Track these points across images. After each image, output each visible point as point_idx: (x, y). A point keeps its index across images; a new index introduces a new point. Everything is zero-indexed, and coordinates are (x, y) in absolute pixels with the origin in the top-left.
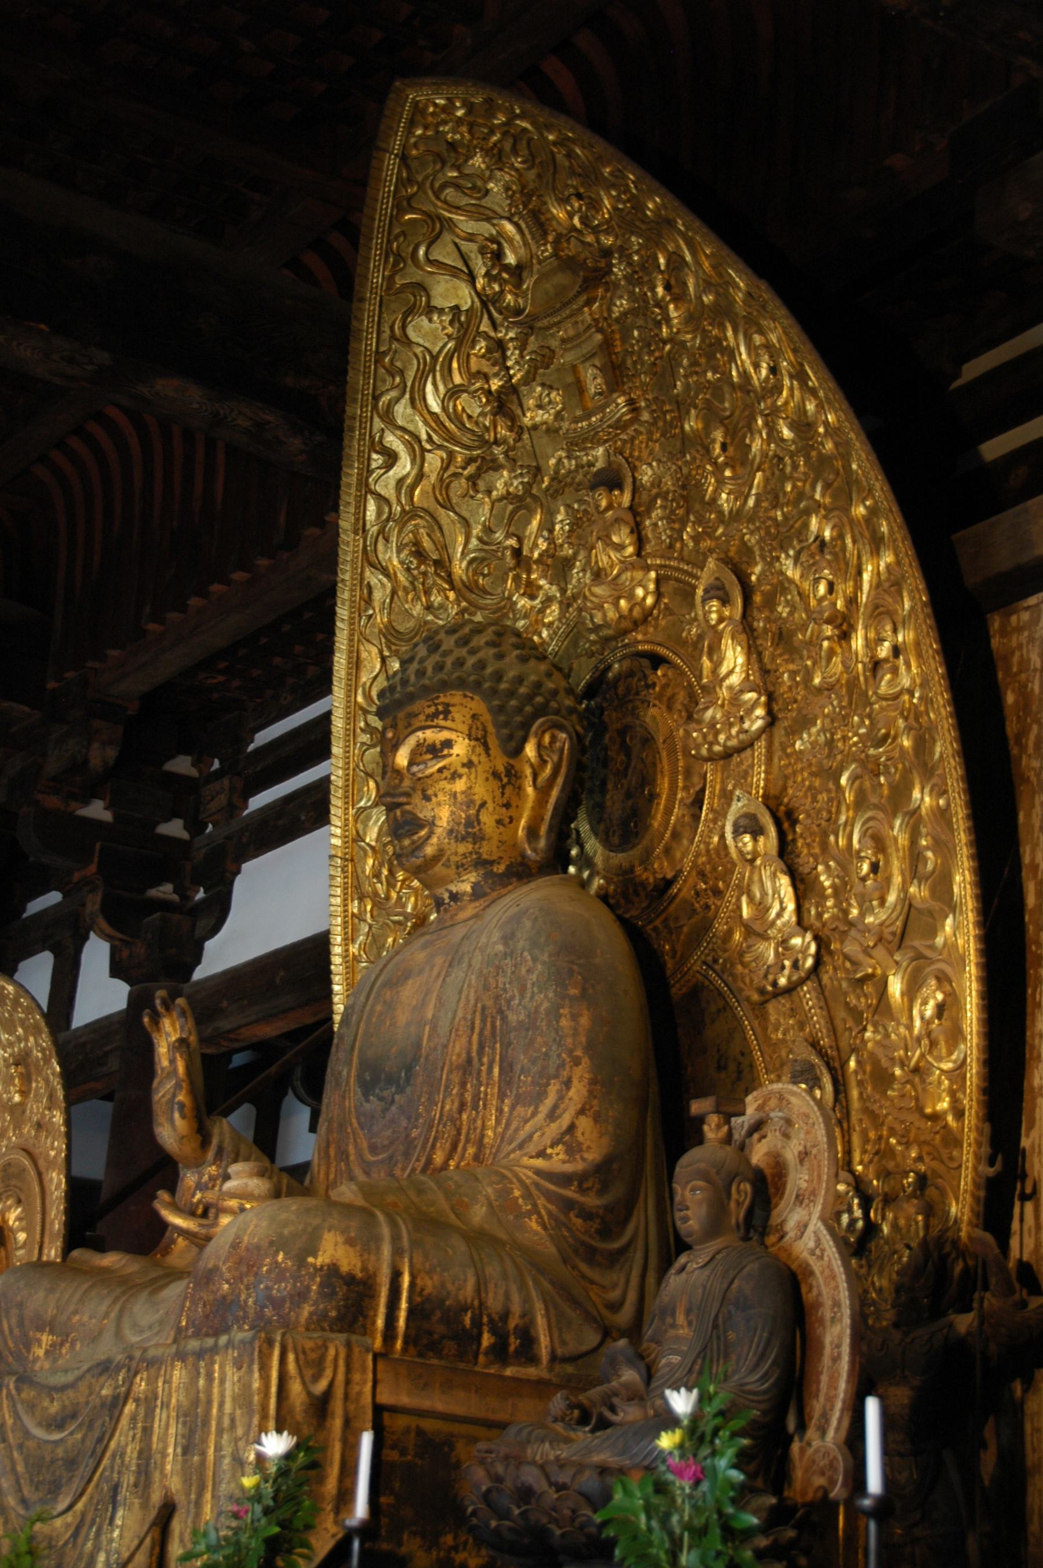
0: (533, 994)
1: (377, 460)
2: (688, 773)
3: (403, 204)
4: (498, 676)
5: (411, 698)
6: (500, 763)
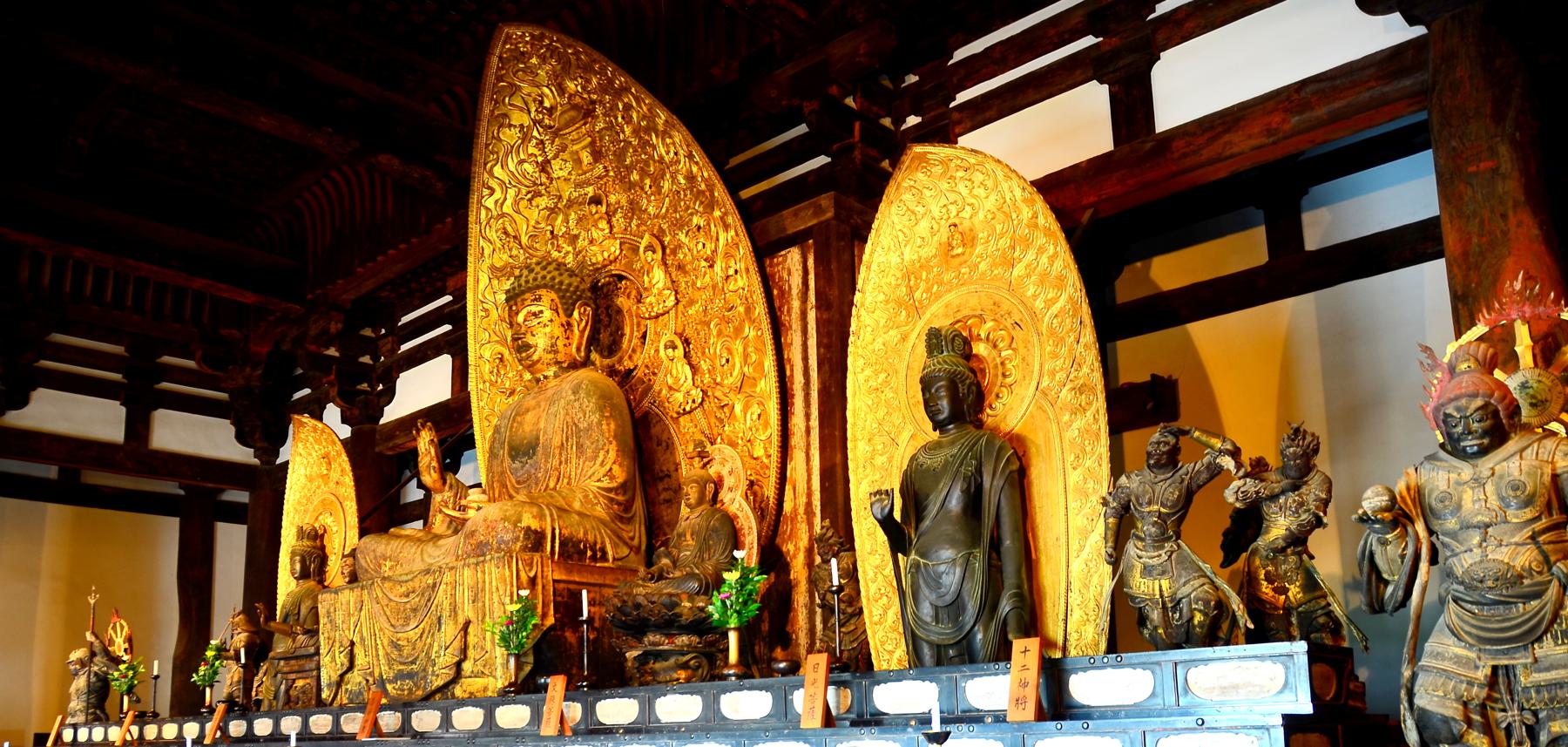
0: (588, 413)
1: (486, 192)
2: (638, 325)
3: (500, 79)
4: (561, 283)
5: (523, 293)
6: (564, 319)
